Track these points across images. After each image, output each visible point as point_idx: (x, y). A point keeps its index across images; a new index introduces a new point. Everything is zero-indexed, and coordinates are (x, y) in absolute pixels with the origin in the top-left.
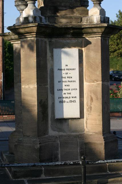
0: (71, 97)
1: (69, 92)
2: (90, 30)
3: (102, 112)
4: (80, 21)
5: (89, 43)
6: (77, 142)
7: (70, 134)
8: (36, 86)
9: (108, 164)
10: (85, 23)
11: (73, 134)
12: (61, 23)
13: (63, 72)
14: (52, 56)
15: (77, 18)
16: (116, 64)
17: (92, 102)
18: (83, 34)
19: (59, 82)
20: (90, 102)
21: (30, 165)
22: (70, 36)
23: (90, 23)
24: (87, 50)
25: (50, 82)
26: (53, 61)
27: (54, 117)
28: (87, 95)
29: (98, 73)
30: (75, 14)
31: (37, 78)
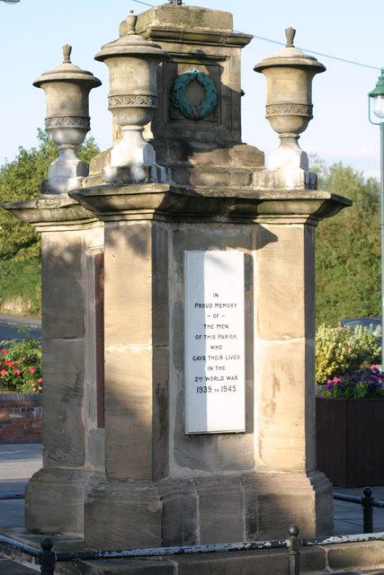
0: (225, 379)
1: (220, 363)
2: (279, 207)
3: (304, 415)
4: (247, 181)
5: (271, 238)
6: (241, 493)
7: (219, 473)
8: (150, 348)
9: (326, 550)
10: (258, 188)
11: (226, 473)
14: (181, 270)
15: (239, 173)
16: (33, 282)
17: (277, 389)
18: (256, 214)
19: (198, 337)
20: (272, 391)
21: (172, 552)
22: (223, 219)
23: (274, 187)
24: (265, 255)
25: (174, 337)
26: (183, 282)
27: (183, 429)
30: (232, 163)
31: (153, 327)
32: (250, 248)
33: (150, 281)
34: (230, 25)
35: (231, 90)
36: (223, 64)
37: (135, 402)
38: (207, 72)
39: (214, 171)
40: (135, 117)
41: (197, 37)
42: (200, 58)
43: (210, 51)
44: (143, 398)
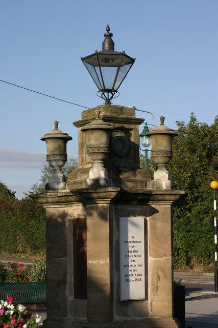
2: (160, 197)
4: (144, 185)
5: (156, 211)
8: (109, 261)
12: (126, 187)
13: (130, 245)
14: (118, 226)
15: (141, 182)
18: (149, 200)
19: (126, 256)
22: (135, 203)
24: (152, 219)
26: (119, 232)
28: (152, 272)
29: (167, 247)
30: (137, 177)
32: (146, 216)
33: (108, 231)
34: (134, 114)
35: (135, 144)
36: (132, 132)
37: (101, 286)
38: (124, 135)
39: (131, 181)
40: (100, 157)
41: (122, 120)
42: (122, 129)
43: (126, 126)
44: (105, 284)
